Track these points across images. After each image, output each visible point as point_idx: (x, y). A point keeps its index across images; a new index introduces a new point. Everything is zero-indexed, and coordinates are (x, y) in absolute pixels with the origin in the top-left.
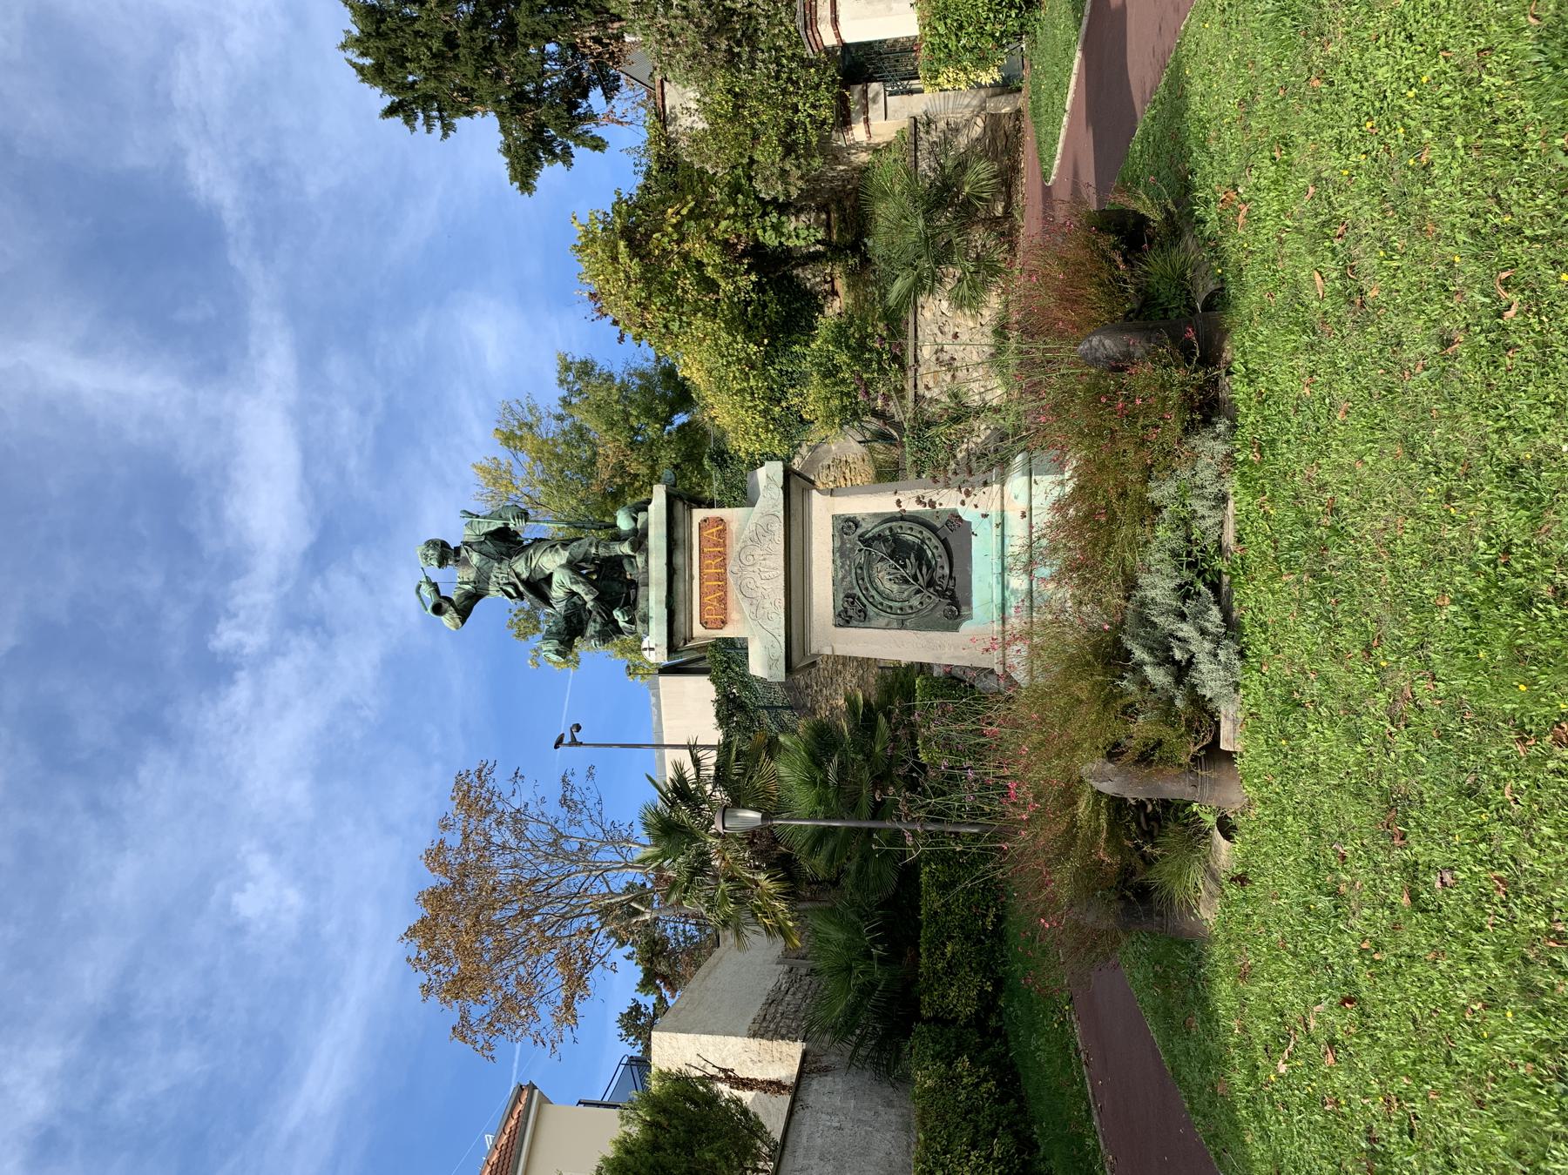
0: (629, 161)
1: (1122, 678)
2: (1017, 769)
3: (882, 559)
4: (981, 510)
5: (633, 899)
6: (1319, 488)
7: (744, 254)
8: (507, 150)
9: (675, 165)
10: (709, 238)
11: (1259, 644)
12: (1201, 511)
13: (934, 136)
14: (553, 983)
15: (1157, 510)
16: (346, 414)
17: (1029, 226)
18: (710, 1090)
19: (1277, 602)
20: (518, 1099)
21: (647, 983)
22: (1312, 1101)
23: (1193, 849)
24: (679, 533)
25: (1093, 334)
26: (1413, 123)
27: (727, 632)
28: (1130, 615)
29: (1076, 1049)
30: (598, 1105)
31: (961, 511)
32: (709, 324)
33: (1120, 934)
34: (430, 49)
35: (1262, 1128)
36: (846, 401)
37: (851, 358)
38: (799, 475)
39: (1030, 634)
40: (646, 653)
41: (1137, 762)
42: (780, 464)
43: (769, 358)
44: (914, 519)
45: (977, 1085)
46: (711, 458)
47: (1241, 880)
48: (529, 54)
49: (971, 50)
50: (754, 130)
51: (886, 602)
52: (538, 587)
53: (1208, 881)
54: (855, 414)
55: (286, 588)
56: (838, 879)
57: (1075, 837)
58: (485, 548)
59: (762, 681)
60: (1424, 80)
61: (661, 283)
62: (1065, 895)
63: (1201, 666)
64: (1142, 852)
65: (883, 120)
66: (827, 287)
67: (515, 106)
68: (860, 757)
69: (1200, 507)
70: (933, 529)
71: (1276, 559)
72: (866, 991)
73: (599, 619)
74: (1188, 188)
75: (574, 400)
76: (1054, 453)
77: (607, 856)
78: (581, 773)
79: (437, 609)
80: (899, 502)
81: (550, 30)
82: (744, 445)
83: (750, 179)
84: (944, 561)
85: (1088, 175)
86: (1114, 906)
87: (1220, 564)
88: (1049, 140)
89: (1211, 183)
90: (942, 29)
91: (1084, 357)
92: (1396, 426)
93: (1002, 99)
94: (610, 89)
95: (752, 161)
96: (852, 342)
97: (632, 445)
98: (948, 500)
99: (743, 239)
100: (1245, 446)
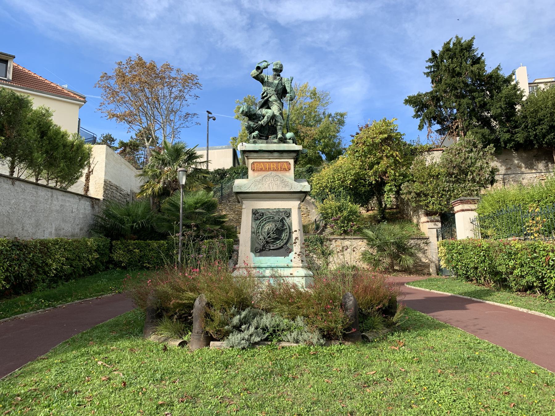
0: (415, 138)
3: (276, 226)
5: (153, 138)
6: (301, 373)
7: (382, 179)
8: (419, 95)
9: (413, 155)
10: (388, 167)
11: (247, 354)
12: (293, 334)
13: (422, 245)
14: (122, 110)
15: (293, 319)
16: (327, 37)
17: (391, 278)
18: (85, 166)
19: (262, 360)
20: (81, 97)
21: (123, 144)
22: (89, 373)
23: (175, 333)
24: (285, 155)
25: (354, 298)
26: (426, 402)
27: (250, 172)
29: (102, 295)
30: (79, 126)
31: (293, 253)
32: (358, 167)
33: (145, 308)
34: (456, 67)
35: (78, 357)
36: (330, 215)
37: (345, 217)
38: (305, 197)
39: (250, 276)
40: (241, 144)
42: (309, 190)
43: (346, 188)
44: (290, 237)
45: (88, 260)
46: (310, 167)
47: (165, 349)
48: (453, 103)
49: (452, 258)
50: (425, 182)
51: (261, 227)
52: (266, 104)
53: (165, 338)
55: (265, 15)
56: (160, 212)
57: (179, 292)
58: (280, 85)
59: (234, 183)
60: (440, 405)
61: (372, 150)
62: (159, 288)
63: (239, 334)
64: (175, 315)
65: (428, 227)
67: (435, 98)
68: (205, 219)
69: (294, 334)
70: (286, 243)
71: (277, 359)
72: (122, 221)
74: (404, 330)
75: (330, 119)
76: (313, 284)
77: (168, 129)
78: (198, 120)
79: (258, 68)
80: (296, 231)
81: (461, 110)
83: (408, 181)
84: (275, 247)
85: (408, 298)
86: (155, 306)
87: (275, 341)
88: (421, 284)
89: (406, 337)
90: (459, 247)
91: (346, 295)
92: (323, 398)
93: (435, 269)
94: (440, 132)
95: (414, 182)
96: (351, 217)
97: (315, 139)
98: (297, 248)
99: (387, 179)
100: (316, 349)
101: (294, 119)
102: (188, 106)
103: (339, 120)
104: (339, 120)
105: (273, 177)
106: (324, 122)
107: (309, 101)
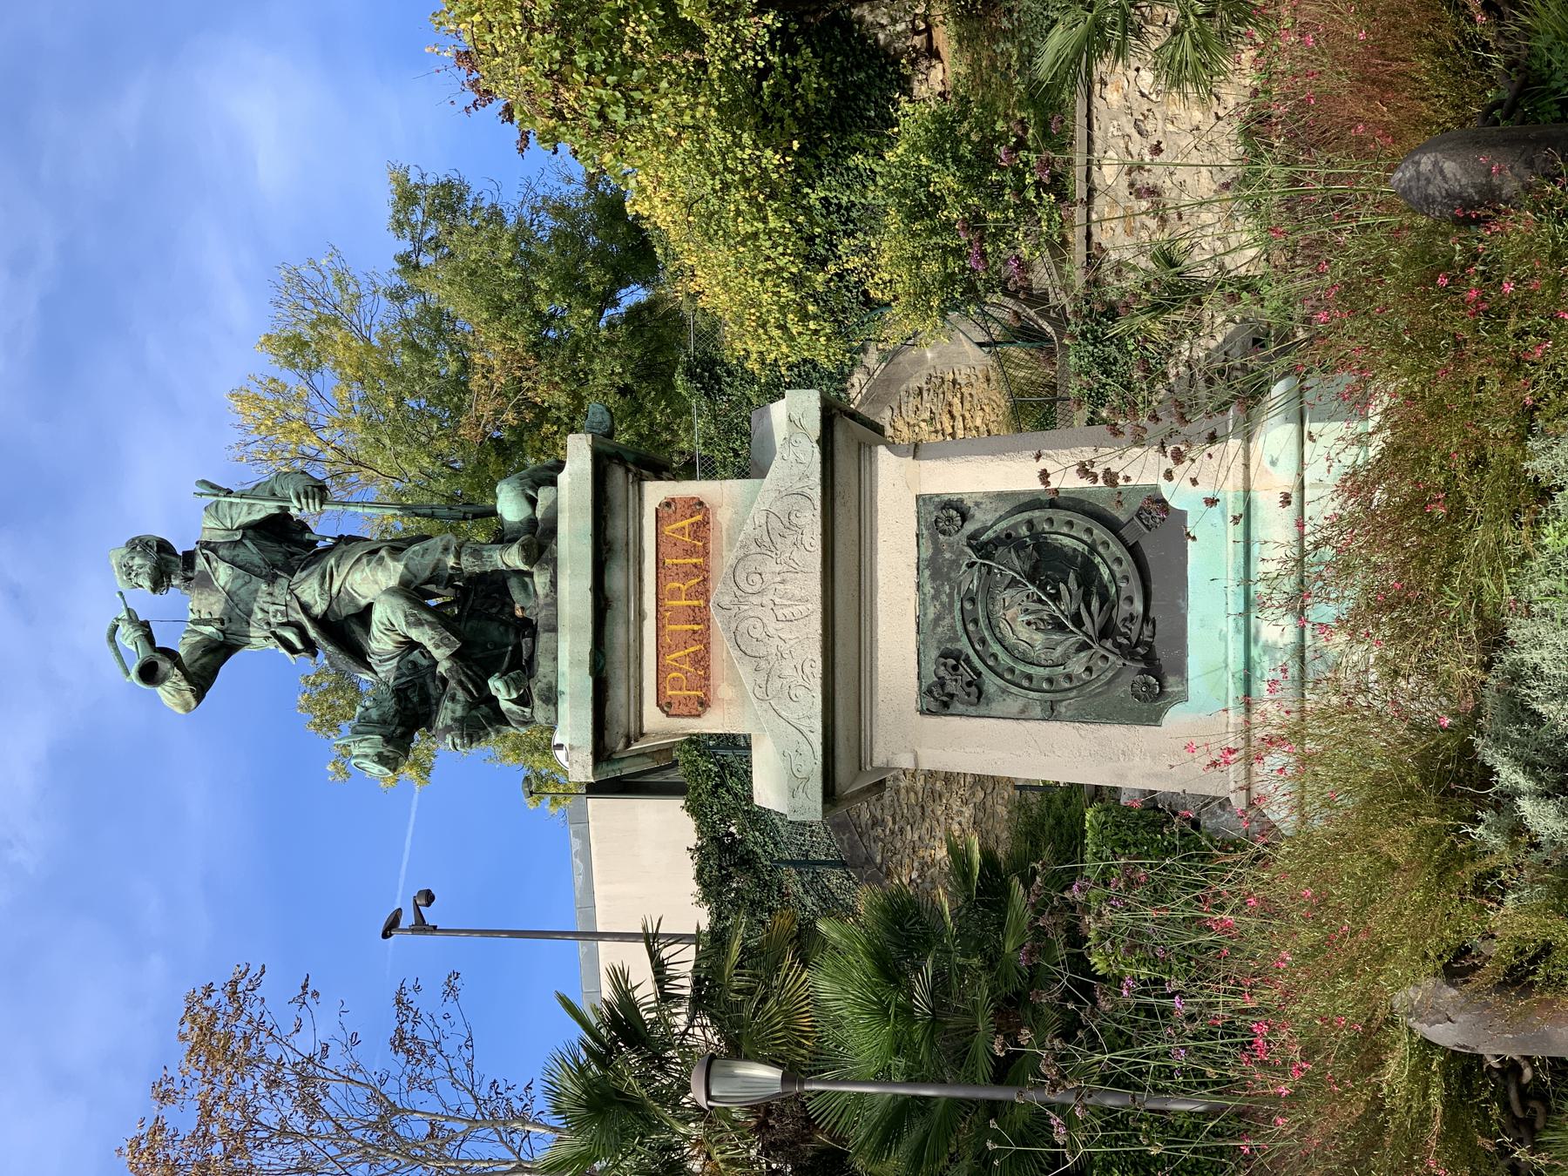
1: (1476, 821)
2: (1270, 995)
3: (1013, 583)
4: (1205, 490)
24: (617, 529)
25: (1423, 149)
27: (712, 723)
28: (1490, 699)
31: (1166, 489)
36: (953, 265)
37: (966, 180)
38: (853, 415)
39: (1297, 734)
41: (1501, 987)
46: (690, 374)
51: (1020, 667)
52: (344, 630)
54: (971, 289)
57: (1380, 1130)
58: (242, 554)
66: (918, 41)
68: (976, 961)
70: (1112, 525)
73: (461, 695)
75: (426, 260)
76: (1346, 378)
79: (149, 674)
80: (1044, 475)
82: (754, 348)
84: (1133, 588)
91: (1405, 193)
96: (965, 149)
97: (536, 347)
98: (1141, 468)
101: (425, 462)
102: (354, 1040)
103: (433, 214)
104: (433, 214)
105: (740, 597)
106: (440, 292)
107: (328, 379)
